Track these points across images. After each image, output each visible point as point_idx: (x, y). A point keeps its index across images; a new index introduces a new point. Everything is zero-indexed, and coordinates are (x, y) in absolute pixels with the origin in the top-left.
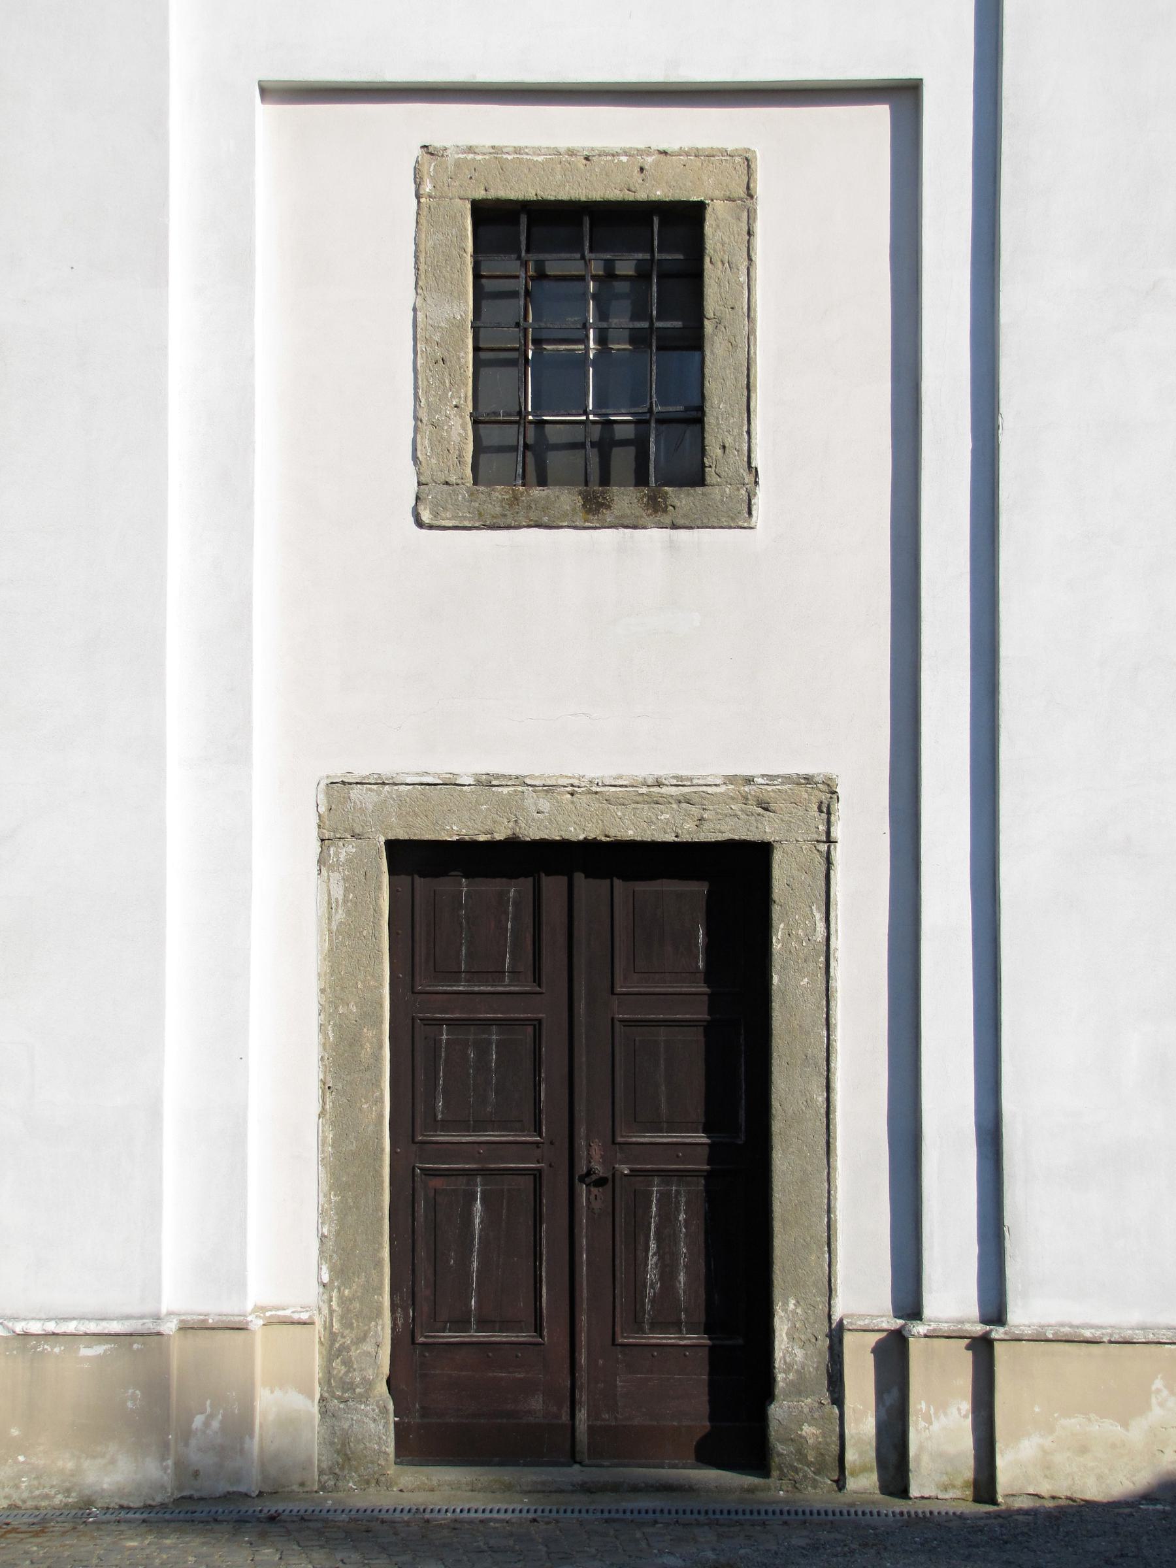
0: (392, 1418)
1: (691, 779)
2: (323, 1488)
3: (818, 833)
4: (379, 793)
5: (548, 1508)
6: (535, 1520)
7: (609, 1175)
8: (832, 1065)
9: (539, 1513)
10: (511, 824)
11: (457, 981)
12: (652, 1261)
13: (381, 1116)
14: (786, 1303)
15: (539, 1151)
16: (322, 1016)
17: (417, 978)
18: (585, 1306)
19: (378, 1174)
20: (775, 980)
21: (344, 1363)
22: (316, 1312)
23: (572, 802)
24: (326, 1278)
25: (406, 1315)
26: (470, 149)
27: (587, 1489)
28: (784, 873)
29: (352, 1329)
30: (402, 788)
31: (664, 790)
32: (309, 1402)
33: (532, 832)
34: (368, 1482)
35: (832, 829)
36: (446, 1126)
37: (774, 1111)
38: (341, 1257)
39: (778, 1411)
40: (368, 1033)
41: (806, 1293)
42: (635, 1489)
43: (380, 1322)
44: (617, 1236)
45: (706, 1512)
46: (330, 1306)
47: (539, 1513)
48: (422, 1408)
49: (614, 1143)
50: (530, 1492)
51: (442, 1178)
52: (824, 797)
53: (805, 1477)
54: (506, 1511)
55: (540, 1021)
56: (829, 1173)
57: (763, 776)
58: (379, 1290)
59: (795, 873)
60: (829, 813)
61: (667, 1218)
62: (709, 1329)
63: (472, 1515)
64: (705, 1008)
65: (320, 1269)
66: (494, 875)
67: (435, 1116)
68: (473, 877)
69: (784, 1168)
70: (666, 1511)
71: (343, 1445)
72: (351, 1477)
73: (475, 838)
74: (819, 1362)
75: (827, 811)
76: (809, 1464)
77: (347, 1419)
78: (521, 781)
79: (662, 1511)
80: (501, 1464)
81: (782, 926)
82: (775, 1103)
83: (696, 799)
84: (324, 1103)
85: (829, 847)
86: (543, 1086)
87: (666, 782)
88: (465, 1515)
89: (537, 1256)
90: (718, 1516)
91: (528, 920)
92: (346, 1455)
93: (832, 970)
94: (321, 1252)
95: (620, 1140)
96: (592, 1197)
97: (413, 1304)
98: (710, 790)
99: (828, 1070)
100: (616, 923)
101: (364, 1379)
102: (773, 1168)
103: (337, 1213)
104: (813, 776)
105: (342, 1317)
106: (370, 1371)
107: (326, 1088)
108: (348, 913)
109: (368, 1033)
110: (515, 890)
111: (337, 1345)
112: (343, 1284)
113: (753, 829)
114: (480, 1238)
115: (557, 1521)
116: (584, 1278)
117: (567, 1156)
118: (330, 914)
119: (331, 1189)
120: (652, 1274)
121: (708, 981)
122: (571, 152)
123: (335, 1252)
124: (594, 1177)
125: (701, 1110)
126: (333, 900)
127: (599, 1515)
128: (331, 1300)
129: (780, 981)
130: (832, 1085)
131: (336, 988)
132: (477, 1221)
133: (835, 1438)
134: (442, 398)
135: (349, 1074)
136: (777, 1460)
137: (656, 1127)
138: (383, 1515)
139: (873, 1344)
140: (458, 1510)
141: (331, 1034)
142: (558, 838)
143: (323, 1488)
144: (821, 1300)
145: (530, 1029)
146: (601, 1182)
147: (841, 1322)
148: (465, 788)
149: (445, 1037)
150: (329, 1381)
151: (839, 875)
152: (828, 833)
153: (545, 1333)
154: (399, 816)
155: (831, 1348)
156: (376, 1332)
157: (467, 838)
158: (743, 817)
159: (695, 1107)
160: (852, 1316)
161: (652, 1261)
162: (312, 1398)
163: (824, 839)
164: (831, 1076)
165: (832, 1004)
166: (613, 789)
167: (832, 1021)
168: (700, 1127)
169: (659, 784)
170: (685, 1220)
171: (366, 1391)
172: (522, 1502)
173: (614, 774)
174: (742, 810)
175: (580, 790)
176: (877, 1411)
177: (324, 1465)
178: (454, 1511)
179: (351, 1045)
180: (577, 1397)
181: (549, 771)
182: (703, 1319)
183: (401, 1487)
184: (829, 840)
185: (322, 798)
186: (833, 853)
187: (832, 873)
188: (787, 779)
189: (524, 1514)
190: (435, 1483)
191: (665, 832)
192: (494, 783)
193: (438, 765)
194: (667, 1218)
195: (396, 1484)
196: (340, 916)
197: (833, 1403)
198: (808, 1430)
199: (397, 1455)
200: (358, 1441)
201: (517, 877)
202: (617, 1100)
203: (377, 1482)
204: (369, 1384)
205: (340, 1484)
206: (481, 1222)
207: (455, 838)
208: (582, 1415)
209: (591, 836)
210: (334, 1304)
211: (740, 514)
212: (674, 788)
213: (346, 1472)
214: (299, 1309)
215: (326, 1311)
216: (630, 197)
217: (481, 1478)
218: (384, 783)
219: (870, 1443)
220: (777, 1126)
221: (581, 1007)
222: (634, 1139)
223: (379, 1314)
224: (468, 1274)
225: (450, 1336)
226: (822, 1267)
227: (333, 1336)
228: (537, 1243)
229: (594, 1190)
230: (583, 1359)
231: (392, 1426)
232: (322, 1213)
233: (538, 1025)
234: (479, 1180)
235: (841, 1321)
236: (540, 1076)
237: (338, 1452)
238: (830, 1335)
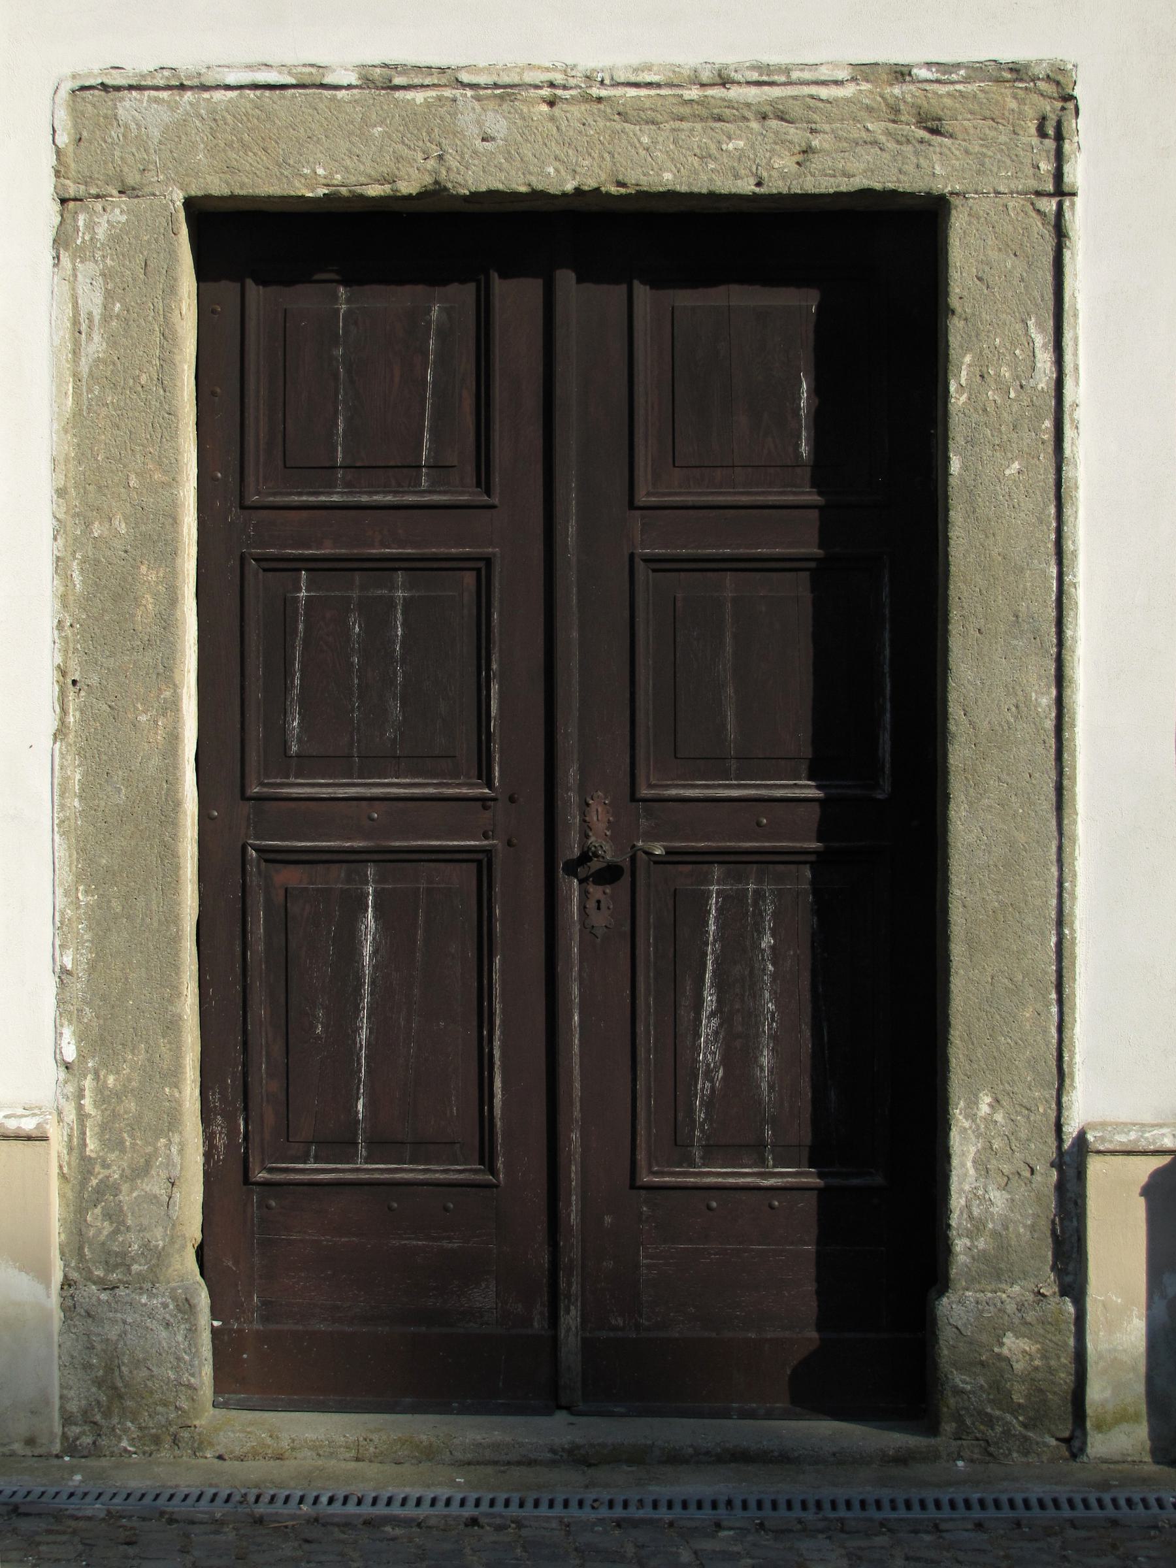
0: (205, 1321)
1: (787, 70)
2: (71, 1448)
3: (1037, 177)
4: (173, 107)
5: (502, 1497)
6: (474, 1522)
7: (624, 860)
8: (1069, 633)
9: (485, 1506)
10: (431, 163)
11: (330, 486)
12: (708, 1026)
14: (973, 1102)
15: (488, 814)
16: (60, 541)
17: (251, 479)
18: (577, 1114)
19: (169, 853)
20: (955, 465)
21: (108, 1216)
22: (52, 1118)
23: (552, 119)
24: (70, 1054)
25: (232, 1132)
27: (579, 1458)
28: (973, 257)
29: (123, 1151)
30: (219, 95)
31: (734, 93)
32: (39, 1289)
34: (157, 1440)
35: (1067, 168)
36: (307, 765)
37: (952, 727)
38: (100, 1010)
39: (957, 1308)
40: (149, 574)
41: (1012, 1083)
42: (674, 1459)
43: (176, 1138)
44: (641, 979)
45: (819, 1505)
46: (80, 1107)
47: (485, 1506)
48: (264, 1303)
49: (633, 798)
50: (469, 1463)
51: (300, 868)
52: (1050, 108)
53: (1007, 1433)
54: (419, 1502)
55: (488, 561)
56: (1060, 848)
57: (929, 65)
58: (174, 1076)
59: (993, 255)
60: (1059, 137)
61: (737, 944)
62: (817, 1157)
63: (351, 1508)
64: (813, 535)
65: (58, 1035)
66: (400, 280)
67: (285, 746)
68: (361, 282)
69: (971, 838)
70: (738, 1503)
71: (109, 1370)
72: (125, 1430)
73: (359, 190)
74: (1036, 1216)
75: (1055, 134)
76: (1015, 1409)
77: (114, 1321)
78: (450, 77)
79: (729, 1503)
80: (414, 1409)
81: (968, 359)
82: (955, 710)
83: (796, 110)
84: (64, 711)
85: (1060, 206)
86: (495, 688)
87: (738, 77)
88: (337, 1508)
89: (484, 1017)
90: (842, 1513)
91: (466, 364)
92: (115, 1388)
93: (1067, 445)
94: (61, 1002)
95: (644, 792)
96: (592, 905)
97: (246, 1108)
98: (824, 92)
99: (1060, 644)
100: (639, 390)
101: (146, 1245)
102: (952, 838)
103: (89, 928)
104: (1027, 66)
105: (104, 1127)
106: (158, 1232)
107: (67, 682)
108: (112, 341)
109: (149, 574)
110: (441, 308)
111: (94, 1182)
112: (104, 1064)
113: (910, 168)
114: (373, 983)
115: (519, 1524)
116: (576, 1060)
117: (542, 827)
118: (76, 344)
119: (79, 878)
120: (708, 1051)
121: (818, 482)
123: (89, 1003)
124: (595, 865)
125: (805, 734)
126: (83, 316)
127: (604, 1512)
128: (80, 1094)
129: (965, 468)
130: (1068, 671)
132: (367, 950)
133: (1066, 1360)
135: (112, 654)
136: (952, 1401)
137: (715, 766)
138: (176, 1507)
139: (1144, 1179)
140: (324, 1500)
141: (77, 577)
142: (523, 189)
143: (71, 1448)
144: (1043, 1095)
145: (469, 578)
146: (610, 875)
147: (1081, 1137)
148: (341, 94)
149: (303, 594)
150: (81, 1248)
151: (1080, 258)
152: (1059, 176)
153: (500, 1164)
154: (211, 151)
155: (1060, 1187)
156: (168, 1157)
157: (344, 191)
158: (891, 145)
159: (795, 732)
160: (1103, 1125)
161: (708, 1026)
162: (43, 1276)
163: (1050, 187)
164: (1067, 656)
165: (1068, 511)
166: (632, 92)
167: (1068, 546)
168: (804, 768)
169: (724, 81)
170: (773, 948)
171: (151, 1269)
172: (452, 1483)
173: (635, 61)
174: (888, 133)
175: (566, 94)
176: (1149, 1307)
177: (73, 1407)
178: (316, 1499)
179: (117, 598)
180: (563, 1285)
181: (508, 59)
182: (808, 1140)
183: (221, 1450)
184: (1061, 191)
185: (63, 117)
186: (1067, 215)
187: (1067, 254)
188: (977, 71)
189: (454, 1509)
190: (285, 1444)
191: (737, 176)
192: (398, 81)
193: (286, 50)
194: (737, 944)
195: (211, 1444)
196: (96, 346)
197: (1064, 1291)
198: (1014, 1345)
199: (218, 1390)
200: (137, 1364)
201: (444, 282)
202: (640, 716)
203: (176, 1441)
204: (158, 1258)
205: (104, 1442)
206: (375, 953)
207: (321, 191)
208: (571, 1319)
209: (590, 184)
210: (87, 1102)
212: (753, 91)
213: (115, 1420)
214: (20, 1111)
215: (71, 1116)
217: (375, 1437)
218: (182, 87)
219: (1134, 1369)
220: (959, 755)
221: (570, 531)
222: (673, 792)
223: (173, 1121)
224: (351, 1052)
225: (316, 1170)
226: (1045, 1031)
227: (86, 1165)
228: (483, 993)
229: (596, 891)
230: (573, 1215)
231: (206, 1338)
232: (62, 927)
233: (483, 567)
234: (370, 871)
235: (1082, 1135)
236: (489, 668)
237: (99, 1383)
238: (1059, 1163)
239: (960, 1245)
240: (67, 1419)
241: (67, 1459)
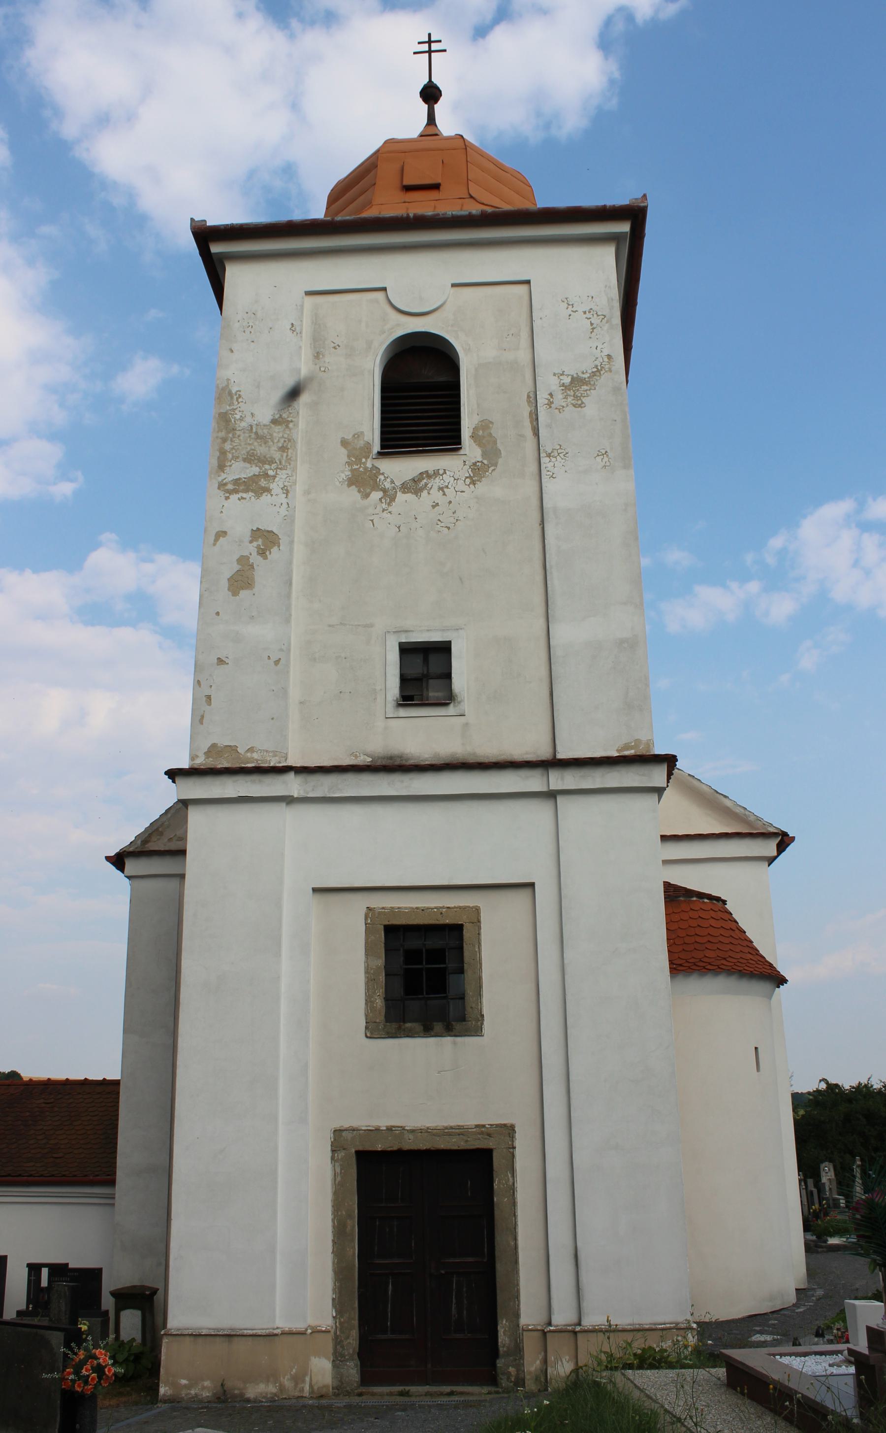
12: (454, 1306)
13: (354, 1254)
26: (383, 908)
33: (406, 1147)
38: (339, 1305)
39: (500, 1363)
122: (417, 908)
131: (337, 1205)
134: (374, 993)
161: (454, 1306)
188: (497, 1125)
196: (339, 1179)
211: (477, 1031)
216: (437, 922)
239: (501, 1349)
240: (333, 1388)
241: (443, 1272)
